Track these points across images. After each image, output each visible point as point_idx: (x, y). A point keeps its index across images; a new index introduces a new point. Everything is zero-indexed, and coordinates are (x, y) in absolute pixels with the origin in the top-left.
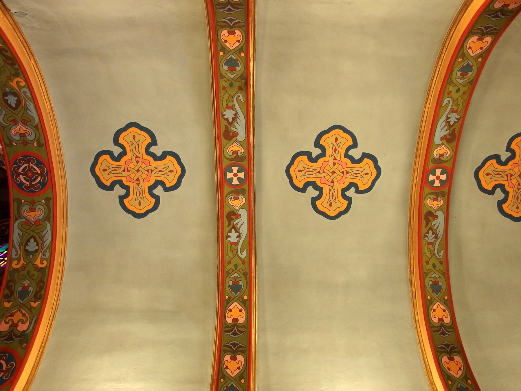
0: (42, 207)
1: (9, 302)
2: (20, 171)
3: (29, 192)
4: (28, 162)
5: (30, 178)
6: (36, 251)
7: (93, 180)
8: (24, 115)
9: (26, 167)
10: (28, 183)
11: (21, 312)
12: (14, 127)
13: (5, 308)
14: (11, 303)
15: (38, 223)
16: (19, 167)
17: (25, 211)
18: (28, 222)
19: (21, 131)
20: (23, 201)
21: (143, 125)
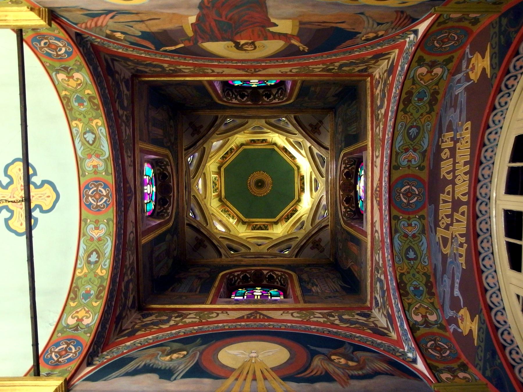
0: (88, 169)
1: (88, 94)
2: (105, 199)
3: (99, 181)
4: (97, 206)
5: (97, 193)
6: (85, 133)
7: (58, 189)
8: (89, 245)
9: (100, 201)
10: (100, 188)
12: (101, 235)
15: (90, 156)
16: (105, 202)
17: (102, 167)
18: (98, 156)
19: (96, 231)
20: (104, 173)
21: (13, 234)
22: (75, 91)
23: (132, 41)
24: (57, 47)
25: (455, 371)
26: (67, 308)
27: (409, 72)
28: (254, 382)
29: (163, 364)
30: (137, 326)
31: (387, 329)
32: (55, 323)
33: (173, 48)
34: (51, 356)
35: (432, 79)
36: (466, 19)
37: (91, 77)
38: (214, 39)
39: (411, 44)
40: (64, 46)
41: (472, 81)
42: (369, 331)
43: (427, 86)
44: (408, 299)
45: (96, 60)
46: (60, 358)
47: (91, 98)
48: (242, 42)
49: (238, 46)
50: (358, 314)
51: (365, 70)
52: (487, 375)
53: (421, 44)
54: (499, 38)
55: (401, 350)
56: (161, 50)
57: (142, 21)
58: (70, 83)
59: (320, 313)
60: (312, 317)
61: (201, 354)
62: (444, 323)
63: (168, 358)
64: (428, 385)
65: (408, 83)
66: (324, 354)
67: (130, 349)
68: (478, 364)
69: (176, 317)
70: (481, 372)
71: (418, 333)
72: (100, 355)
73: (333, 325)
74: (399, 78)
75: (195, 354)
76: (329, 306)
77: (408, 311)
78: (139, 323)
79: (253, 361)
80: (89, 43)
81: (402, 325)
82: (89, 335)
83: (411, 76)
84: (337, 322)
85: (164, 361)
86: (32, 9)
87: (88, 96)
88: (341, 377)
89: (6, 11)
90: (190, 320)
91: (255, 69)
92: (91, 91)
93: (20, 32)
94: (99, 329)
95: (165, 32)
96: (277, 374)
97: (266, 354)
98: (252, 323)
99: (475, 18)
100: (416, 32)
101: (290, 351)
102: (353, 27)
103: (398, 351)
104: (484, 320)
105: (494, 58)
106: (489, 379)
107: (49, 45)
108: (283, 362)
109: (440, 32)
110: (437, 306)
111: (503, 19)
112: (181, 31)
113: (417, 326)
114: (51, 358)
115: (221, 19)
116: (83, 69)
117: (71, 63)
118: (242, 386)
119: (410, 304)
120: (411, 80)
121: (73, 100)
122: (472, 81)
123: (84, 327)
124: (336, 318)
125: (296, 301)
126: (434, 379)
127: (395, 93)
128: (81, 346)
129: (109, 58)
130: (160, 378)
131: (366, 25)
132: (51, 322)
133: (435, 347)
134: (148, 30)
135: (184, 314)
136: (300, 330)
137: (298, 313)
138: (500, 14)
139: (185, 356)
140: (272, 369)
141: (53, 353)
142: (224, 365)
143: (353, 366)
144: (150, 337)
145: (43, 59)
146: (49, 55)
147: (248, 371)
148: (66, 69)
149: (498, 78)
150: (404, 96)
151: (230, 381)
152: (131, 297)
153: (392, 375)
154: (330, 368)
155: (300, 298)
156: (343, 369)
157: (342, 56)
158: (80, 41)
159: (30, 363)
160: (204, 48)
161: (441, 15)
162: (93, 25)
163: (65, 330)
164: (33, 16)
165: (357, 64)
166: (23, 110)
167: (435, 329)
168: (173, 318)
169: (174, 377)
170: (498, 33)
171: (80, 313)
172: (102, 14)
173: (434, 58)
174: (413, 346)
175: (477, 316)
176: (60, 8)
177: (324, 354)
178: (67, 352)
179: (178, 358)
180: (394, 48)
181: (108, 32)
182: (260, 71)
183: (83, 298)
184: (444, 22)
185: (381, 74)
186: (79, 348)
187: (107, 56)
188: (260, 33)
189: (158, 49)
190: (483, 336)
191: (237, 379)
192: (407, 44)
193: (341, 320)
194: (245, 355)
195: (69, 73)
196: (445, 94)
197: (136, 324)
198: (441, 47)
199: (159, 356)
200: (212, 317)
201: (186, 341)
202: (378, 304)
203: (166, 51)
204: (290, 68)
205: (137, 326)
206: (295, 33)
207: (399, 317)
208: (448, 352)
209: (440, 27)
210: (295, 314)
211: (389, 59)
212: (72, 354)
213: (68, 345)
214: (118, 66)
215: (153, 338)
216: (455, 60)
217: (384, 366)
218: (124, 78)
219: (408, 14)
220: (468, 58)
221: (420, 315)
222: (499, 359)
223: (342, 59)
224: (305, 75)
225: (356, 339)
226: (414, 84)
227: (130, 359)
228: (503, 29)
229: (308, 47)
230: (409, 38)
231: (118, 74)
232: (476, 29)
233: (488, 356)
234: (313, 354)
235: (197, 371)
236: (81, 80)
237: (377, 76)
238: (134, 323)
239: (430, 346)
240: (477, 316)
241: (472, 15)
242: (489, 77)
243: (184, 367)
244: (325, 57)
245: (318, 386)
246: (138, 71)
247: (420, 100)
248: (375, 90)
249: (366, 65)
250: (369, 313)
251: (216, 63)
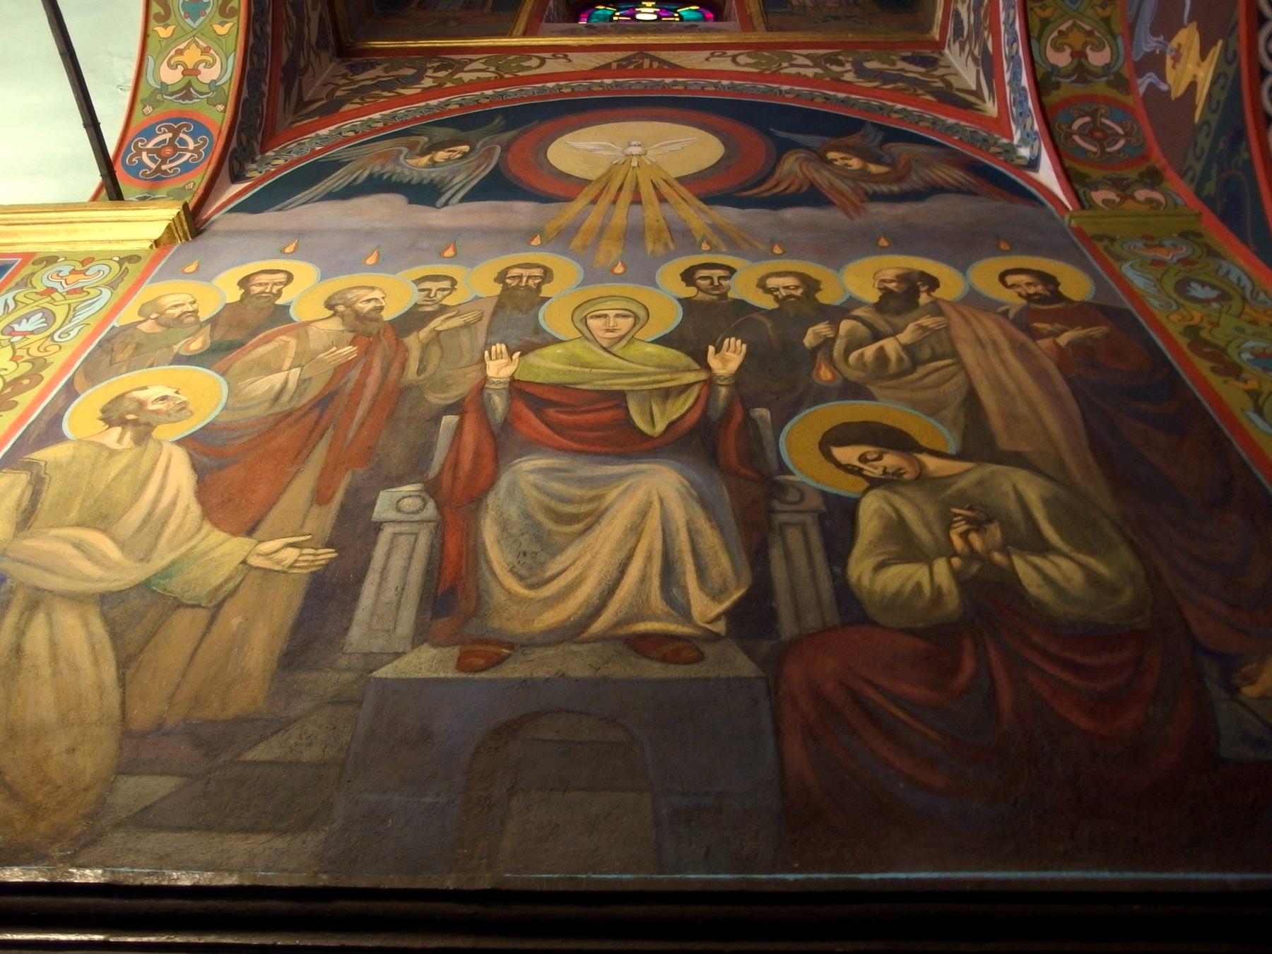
25: (1128, 186)
26: (152, 42)
28: (636, 208)
29: (415, 174)
30: (339, 93)
31: (978, 93)
32: (131, 85)
34: (140, 160)
42: (929, 97)
44: (1044, 8)
46: (164, 162)
50: (905, 59)
52: (1205, 193)
55: (1005, 141)
59: (807, 56)
60: (785, 65)
61: (506, 149)
62: (1126, 72)
63: (425, 160)
64: (1056, 215)
66: (808, 148)
67: (330, 142)
68: (1190, 168)
69: (437, 70)
70: (1194, 186)
71: (1054, 98)
72: (258, 157)
73: (838, 82)
75: (490, 152)
76: (831, 38)
77: (1039, 40)
78: (344, 85)
79: (634, 164)
81: (1016, 76)
82: (221, 107)
84: (849, 77)
85: (416, 166)
88: (848, 199)
90: (474, 76)
94: (245, 94)
96: (690, 190)
97: (667, 149)
98: (632, 80)
101: (725, 141)
103: (995, 144)
104: (1235, 54)
106: (1209, 202)
108: (707, 165)
110: (1117, 27)
113: (1053, 79)
114: (142, 164)
118: (608, 216)
119: (1045, 22)
123: (206, 89)
124: (848, 66)
125: (747, 24)
126: (1075, 201)
128: (209, 134)
130: (410, 202)
132: (121, 80)
133: (1088, 133)
135: (458, 62)
136: (753, 95)
137: (749, 55)
139: (465, 155)
140: (680, 180)
141: (144, 154)
142: (561, 173)
143: (879, 175)
144: (376, 116)
147: (622, 185)
151: (579, 204)
152: (315, 17)
153: (972, 193)
154: (822, 178)
155: (758, 20)
156: (854, 180)
159: (94, 178)
163: (159, 97)
167: (1100, 87)
168: (430, 73)
169: (443, 200)
171: (186, 53)
174: (1036, 127)
175: (1220, 43)
177: (808, 148)
178: (176, 149)
179: (448, 159)
183: (188, 15)
186: (205, 140)
190: (1222, 96)
191: (594, 202)
193: (860, 71)
194: (614, 150)
197: (338, 87)
199: (402, 157)
200: (529, 68)
201: (467, 124)
202: (962, 29)
204: (544, 70)
205: (339, 93)
207: (1013, 58)
208: (1122, 143)
210: (743, 59)
212: (189, 155)
213: (176, 132)
215: (383, 118)
217: (956, 175)
221: (1068, 51)
222: (1248, 149)
225: (895, 116)
227: (336, 165)
233: (1221, 146)
234: (784, 148)
235: (496, 186)
238: (331, 87)
239: (1081, 127)
240: (1220, 43)
243: (465, 178)
245: (789, 214)
250: (936, 56)
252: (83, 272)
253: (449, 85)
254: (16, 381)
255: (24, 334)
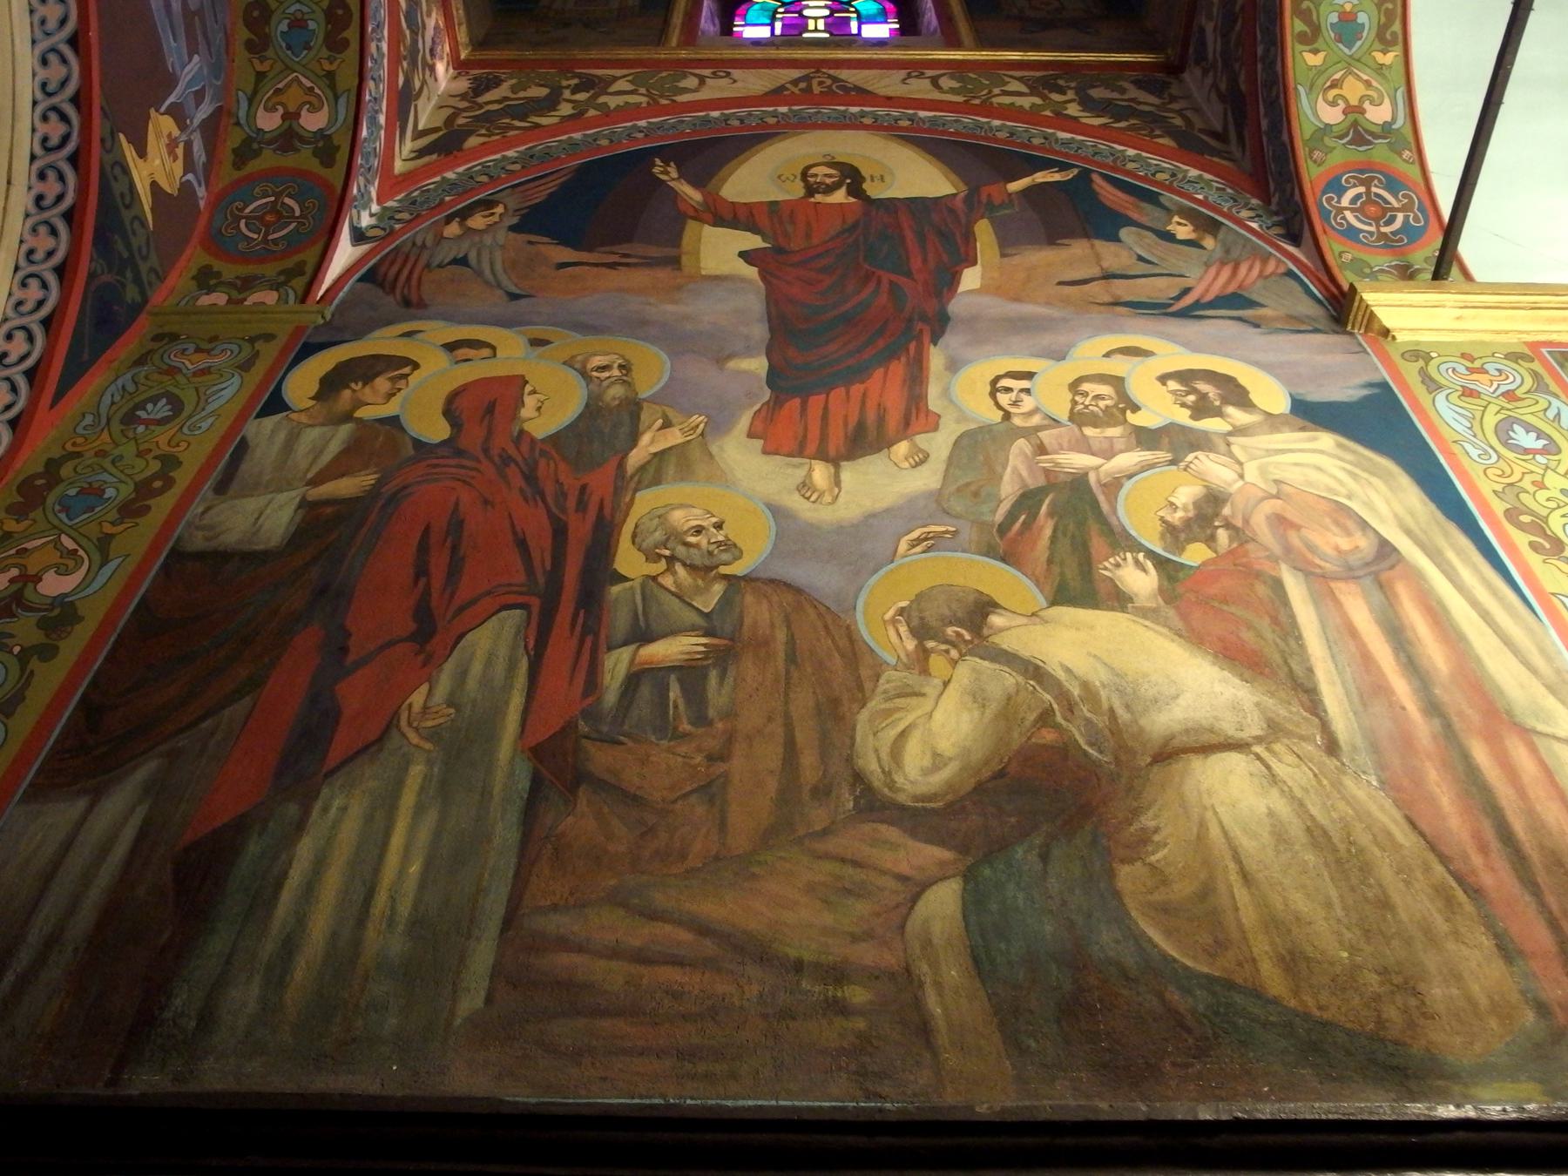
1: (1315, 52)
11: (1359, 78)
13: (1310, 68)
14: (1321, 55)
22: (1351, 64)
23: (1147, 207)
24: (1359, 211)
27: (352, 114)
33: (1041, 177)
35: (278, 91)
36: (232, 285)
37: (1293, 109)
38: (919, 207)
39: (364, 194)
40: (1341, 210)
41: (163, 109)
43: (288, 69)
45: (1269, 152)
47: (1311, 38)
48: (840, 196)
49: (851, 177)
51: (480, 87)
53: (338, 205)
54: (128, 245)
56: (1076, 171)
57: (1108, 276)
58: (1361, 89)
59: (1020, 79)
60: (996, 91)
65: (347, 79)
74: (377, 91)
78: (465, 110)
80: (1273, 207)
83: (342, 101)
86: (1386, 332)
87: (1319, 44)
89: (1453, 331)
91: (809, 90)
92: (1304, 61)
93: (1445, 265)
95: (1054, 236)
99: (210, 290)
100: (359, 236)
102: (531, 248)
105: (127, 192)
107: (1384, 214)
109: (294, 244)
111: (138, 299)
112: (1008, 242)
115: (893, 277)
116: (1307, 136)
117: (1340, 155)
120: (339, 91)
121: (1369, 34)
122: (163, 109)
124: (1071, 95)
127: (379, 40)
129: (1234, 147)
131: (498, 256)
134: (1098, 243)
137: (952, 77)
138: (148, 307)
145: (1414, 172)
146: (1393, 184)
148: (1359, 134)
149: (96, 143)
150: (352, 34)
157: (553, 142)
158: (1294, 221)
160: (953, 177)
161: (303, 300)
162: (1243, 269)
164: (1386, 317)
165: (505, 112)
166: (1508, 57)
170: (140, 262)
172: (1212, 305)
173: (289, 161)
176: (1316, 331)
180: (409, 177)
181: (1209, 242)
182: (795, 82)
184: (290, 274)
185: (430, 81)
187: (1238, 155)
188: (790, 228)
189: (1085, 175)
192: (374, 195)
195: (1355, 124)
196: (227, 45)
198: (278, 195)
200: (685, 90)
203: (1063, 167)
204: (704, 95)
206: (691, 226)
209: (297, 258)
210: (946, 83)
211: (418, 135)
214: (1215, 114)
216: (227, 156)
218: (1205, 72)
219: (390, 299)
220: (194, 172)
223: (554, 131)
224: (658, 65)
226: (330, 76)
228: (129, 274)
229: (653, 175)
230: (372, 215)
231: (1218, 90)
232: (195, 257)
236: (1326, 101)
237: (440, 67)
241: (219, 298)
242: (122, 136)
244: (607, 139)
246: (1157, 88)
247: (298, 23)
248: (441, 24)
249: (480, 106)
251: (922, 114)
252: (208, 352)
253: (592, 113)
254: (147, 482)
255: (147, 423)
